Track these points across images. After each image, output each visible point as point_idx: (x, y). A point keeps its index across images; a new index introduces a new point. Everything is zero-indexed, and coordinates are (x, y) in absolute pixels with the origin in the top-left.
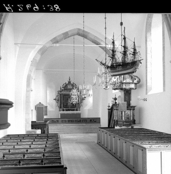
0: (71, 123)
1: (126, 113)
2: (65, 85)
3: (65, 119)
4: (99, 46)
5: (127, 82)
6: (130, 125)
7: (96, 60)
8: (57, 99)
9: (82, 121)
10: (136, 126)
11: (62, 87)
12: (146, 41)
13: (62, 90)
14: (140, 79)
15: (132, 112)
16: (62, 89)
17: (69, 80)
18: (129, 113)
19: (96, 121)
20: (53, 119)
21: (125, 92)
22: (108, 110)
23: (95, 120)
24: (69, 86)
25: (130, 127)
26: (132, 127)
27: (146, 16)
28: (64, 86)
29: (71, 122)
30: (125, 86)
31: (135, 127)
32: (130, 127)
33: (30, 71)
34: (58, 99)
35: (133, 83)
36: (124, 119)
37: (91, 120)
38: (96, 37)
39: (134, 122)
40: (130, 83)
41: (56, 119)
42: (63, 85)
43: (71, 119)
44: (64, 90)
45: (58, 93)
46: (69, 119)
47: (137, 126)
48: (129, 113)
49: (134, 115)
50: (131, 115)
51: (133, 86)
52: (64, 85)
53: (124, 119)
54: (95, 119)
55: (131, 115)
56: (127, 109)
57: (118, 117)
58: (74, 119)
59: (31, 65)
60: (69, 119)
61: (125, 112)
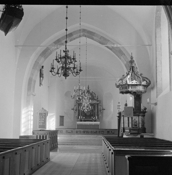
0: (87, 134)
1: (133, 119)
3: (80, 130)
4: (105, 45)
5: (133, 83)
8: (75, 108)
9: (98, 132)
10: (146, 135)
12: (156, 37)
14: (150, 81)
15: (141, 118)
18: (137, 119)
19: (114, 133)
21: (135, 97)
22: (117, 117)
23: (113, 132)
25: (139, 136)
26: (142, 137)
27: (155, 9)
29: (87, 133)
30: (132, 88)
31: (145, 137)
33: (32, 74)
34: (76, 109)
35: (140, 85)
37: (108, 132)
38: (102, 37)
39: (144, 130)
40: (137, 85)
41: (71, 130)
43: (87, 130)
45: (77, 103)
46: (84, 130)
48: (137, 119)
49: (143, 122)
51: (141, 88)
54: (113, 130)
55: (140, 122)
56: (134, 115)
58: (90, 130)
59: (33, 69)
60: (84, 130)
61: (132, 118)
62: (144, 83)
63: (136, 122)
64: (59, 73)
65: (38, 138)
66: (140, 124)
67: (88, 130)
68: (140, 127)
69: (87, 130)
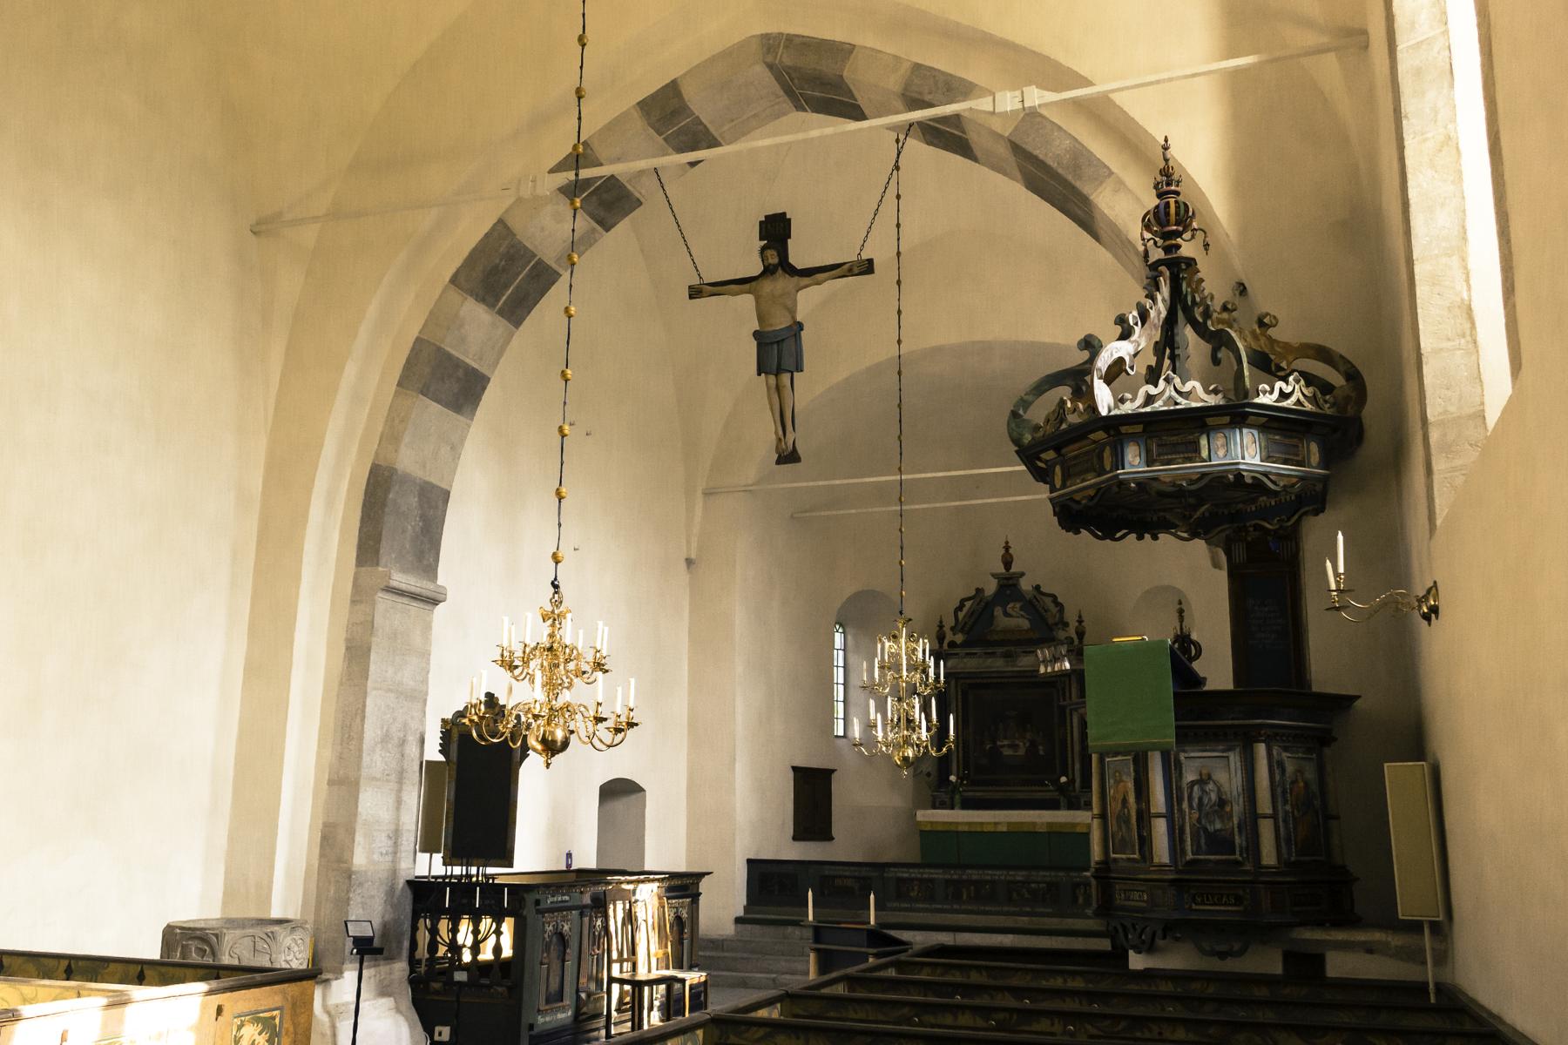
2: (968, 604)
6: (1251, 932)
7: (695, 293)
11: (949, 622)
13: (952, 644)
15: (1275, 766)
16: (949, 637)
17: (1001, 569)
20: (827, 871)
21: (1240, 553)
24: (1006, 614)
25: (1268, 962)
26: (1306, 965)
28: (961, 615)
31: (1339, 965)
32: (1268, 962)
36: (1161, 849)
42: (960, 608)
44: (965, 644)
46: (954, 875)
47: (1369, 949)
50: (1264, 804)
52: (965, 610)
53: (1161, 849)
55: (1264, 804)
57: (1113, 825)
60: (954, 875)
62: (837, 627)
63: (1222, 802)
64: (241, 1020)
65: (655, 987)
66: (1266, 830)
67: (988, 875)
68: (1269, 856)
69: (974, 875)
